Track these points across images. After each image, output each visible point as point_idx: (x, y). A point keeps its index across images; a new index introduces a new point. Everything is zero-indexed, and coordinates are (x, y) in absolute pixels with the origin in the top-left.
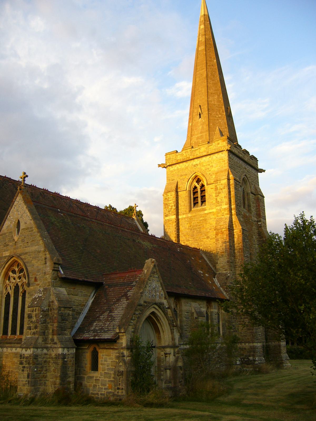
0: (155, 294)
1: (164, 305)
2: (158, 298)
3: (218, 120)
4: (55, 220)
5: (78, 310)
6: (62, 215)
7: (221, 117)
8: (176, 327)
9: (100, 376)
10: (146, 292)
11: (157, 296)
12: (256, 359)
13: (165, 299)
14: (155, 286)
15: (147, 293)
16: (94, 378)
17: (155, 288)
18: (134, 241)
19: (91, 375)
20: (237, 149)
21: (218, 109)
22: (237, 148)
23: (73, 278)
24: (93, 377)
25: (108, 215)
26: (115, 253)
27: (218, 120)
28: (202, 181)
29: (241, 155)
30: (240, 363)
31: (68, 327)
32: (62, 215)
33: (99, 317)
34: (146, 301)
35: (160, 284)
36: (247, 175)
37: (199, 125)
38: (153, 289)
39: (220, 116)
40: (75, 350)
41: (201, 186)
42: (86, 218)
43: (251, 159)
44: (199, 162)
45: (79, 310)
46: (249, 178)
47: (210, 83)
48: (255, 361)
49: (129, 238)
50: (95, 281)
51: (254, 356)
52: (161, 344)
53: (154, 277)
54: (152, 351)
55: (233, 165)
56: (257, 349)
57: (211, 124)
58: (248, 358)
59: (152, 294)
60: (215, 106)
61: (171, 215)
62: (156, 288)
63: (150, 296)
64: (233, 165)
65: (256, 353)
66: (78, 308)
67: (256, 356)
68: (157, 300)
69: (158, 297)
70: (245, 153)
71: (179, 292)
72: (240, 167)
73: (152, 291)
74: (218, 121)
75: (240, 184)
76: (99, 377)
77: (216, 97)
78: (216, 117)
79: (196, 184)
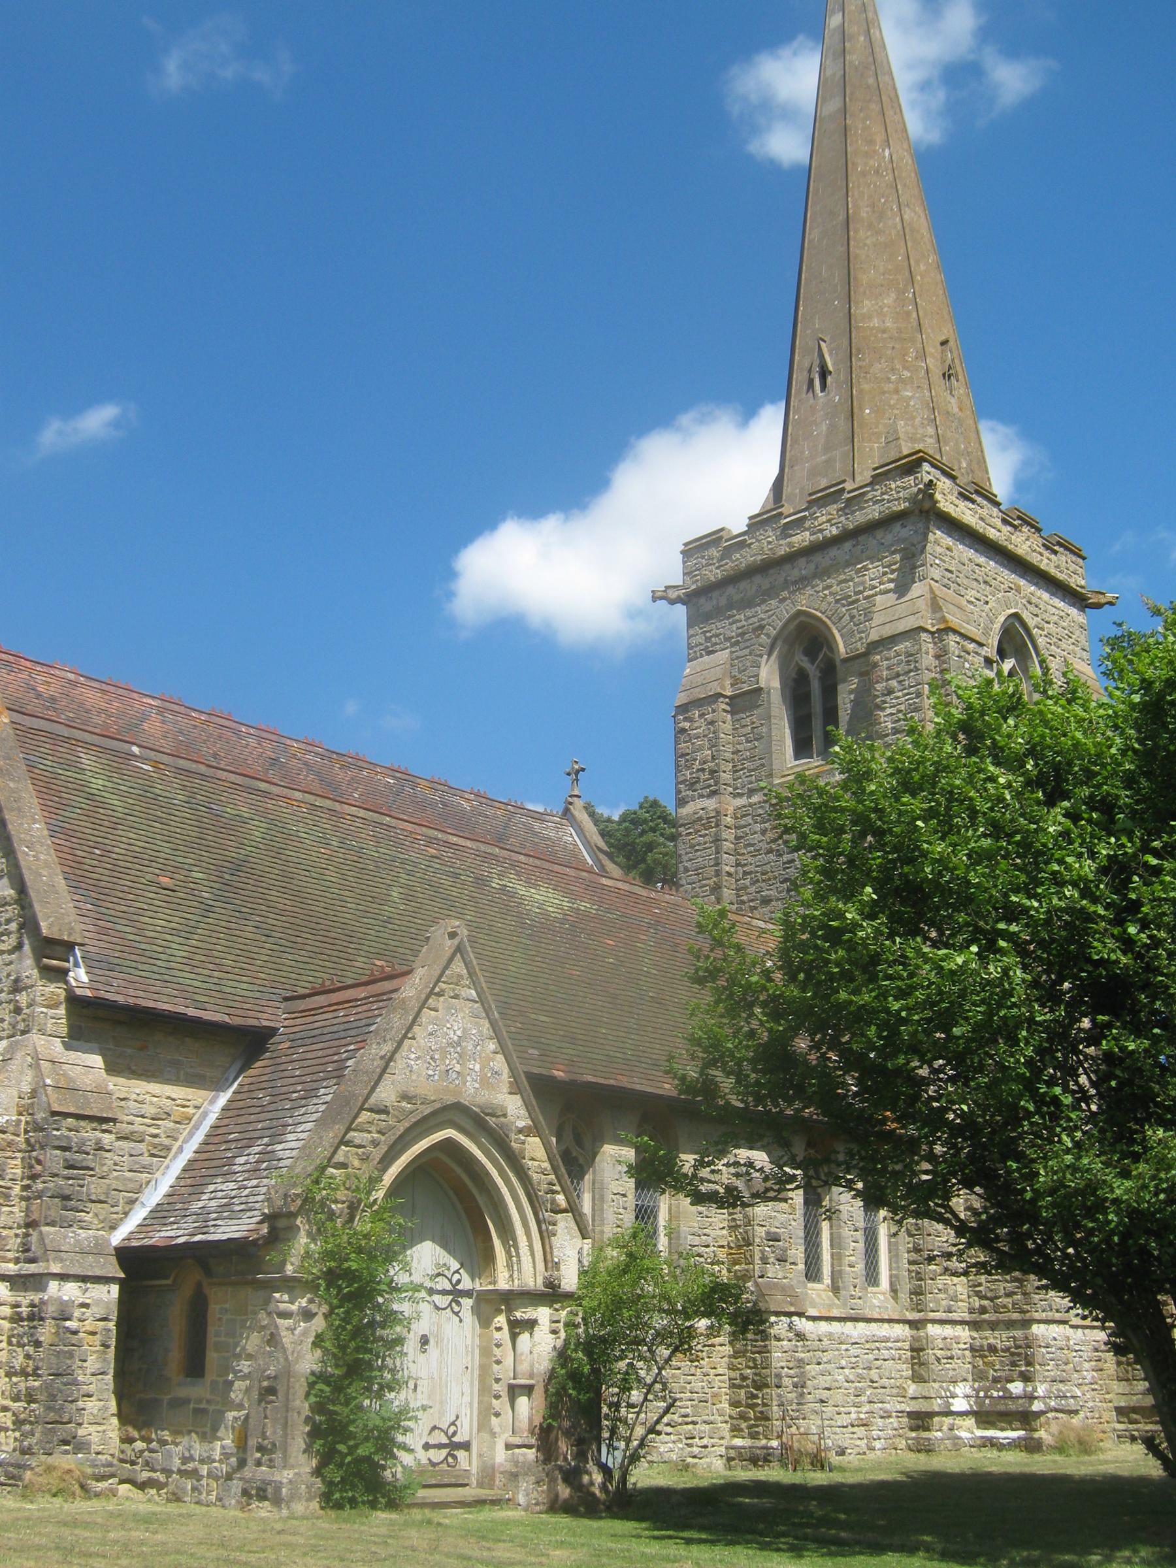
0: (458, 1068)
1: (505, 1116)
2: (477, 1085)
3: (897, 391)
4: (107, 784)
5: (155, 1136)
6: (145, 767)
7: (911, 377)
8: (565, 1211)
9: (208, 1396)
10: (413, 1056)
11: (469, 1078)
12: (1035, 1390)
13: (510, 1093)
14: (459, 1033)
15: (418, 1058)
16: (192, 1406)
17: (459, 1044)
18: (481, 882)
19: (182, 1392)
20: (971, 506)
21: (897, 346)
22: (973, 501)
23: (131, 1001)
24: (187, 1401)
25: (444, 804)
26: (370, 921)
27: (897, 391)
28: (825, 649)
29: (992, 534)
30: (971, 1406)
31: (93, 1197)
32: (145, 767)
33: (230, 1162)
34: (412, 1091)
35: (487, 1025)
36: (1025, 615)
37: (818, 420)
38: (450, 1044)
39: (907, 374)
40: (115, 1289)
41: (822, 666)
42: (263, 786)
43: (1046, 553)
44: (812, 566)
45: (163, 1135)
46: (1035, 631)
47: (865, 245)
48: (1031, 1398)
49: (458, 871)
50: (238, 1021)
51: (1026, 1378)
52: (495, 1283)
53: (456, 997)
54: (456, 1309)
55: (951, 572)
56: (1044, 1350)
57: (867, 411)
58: (1005, 1390)
59: (443, 1068)
60: (885, 336)
61: (702, 796)
62: (464, 1044)
63: (430, 1072)
64: (951, 572)
65: (1038, 1367)
66: (158, 1127)
67: (1039, 1377)
68: (472, 1092)
69: (473, 1080)
70: (1016, 523)
71: (661, 1092)
72: (985, 582)
73: (443, 1052)
74: (895, 397)
75: (985, 651)
76: (208, 1402)
77: (889, 300)
78: (889, 379)
79: (806, 664)
